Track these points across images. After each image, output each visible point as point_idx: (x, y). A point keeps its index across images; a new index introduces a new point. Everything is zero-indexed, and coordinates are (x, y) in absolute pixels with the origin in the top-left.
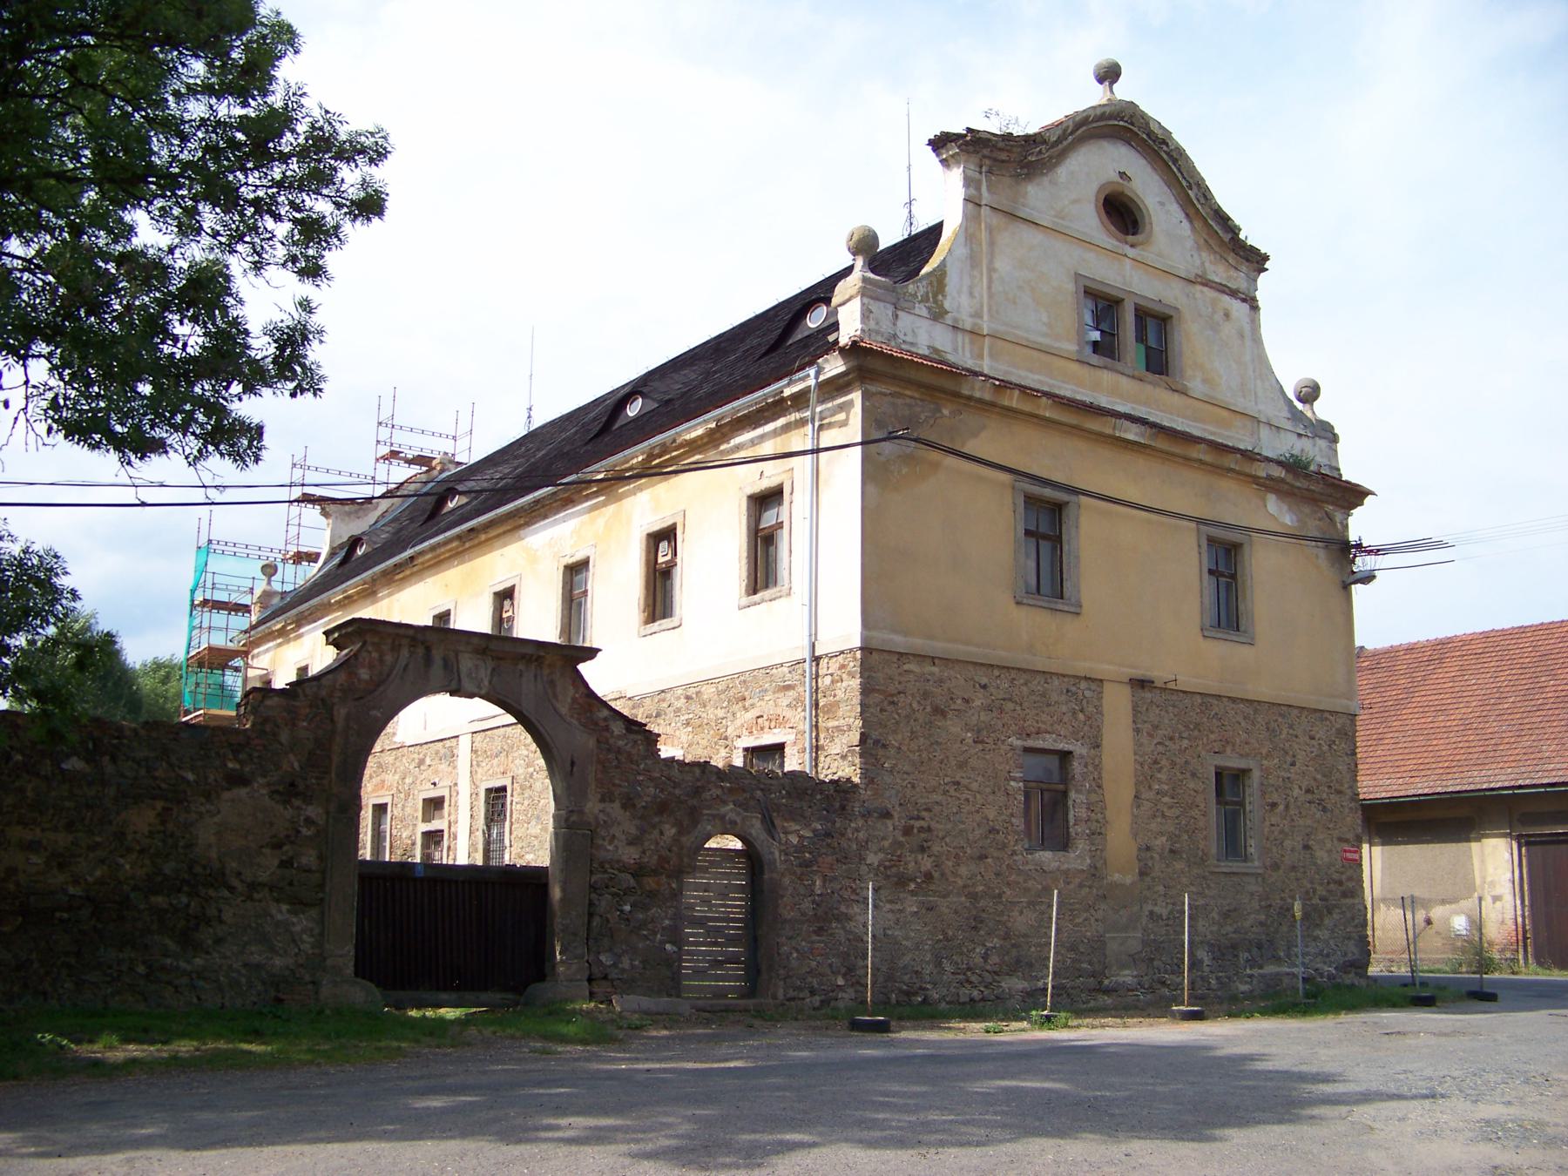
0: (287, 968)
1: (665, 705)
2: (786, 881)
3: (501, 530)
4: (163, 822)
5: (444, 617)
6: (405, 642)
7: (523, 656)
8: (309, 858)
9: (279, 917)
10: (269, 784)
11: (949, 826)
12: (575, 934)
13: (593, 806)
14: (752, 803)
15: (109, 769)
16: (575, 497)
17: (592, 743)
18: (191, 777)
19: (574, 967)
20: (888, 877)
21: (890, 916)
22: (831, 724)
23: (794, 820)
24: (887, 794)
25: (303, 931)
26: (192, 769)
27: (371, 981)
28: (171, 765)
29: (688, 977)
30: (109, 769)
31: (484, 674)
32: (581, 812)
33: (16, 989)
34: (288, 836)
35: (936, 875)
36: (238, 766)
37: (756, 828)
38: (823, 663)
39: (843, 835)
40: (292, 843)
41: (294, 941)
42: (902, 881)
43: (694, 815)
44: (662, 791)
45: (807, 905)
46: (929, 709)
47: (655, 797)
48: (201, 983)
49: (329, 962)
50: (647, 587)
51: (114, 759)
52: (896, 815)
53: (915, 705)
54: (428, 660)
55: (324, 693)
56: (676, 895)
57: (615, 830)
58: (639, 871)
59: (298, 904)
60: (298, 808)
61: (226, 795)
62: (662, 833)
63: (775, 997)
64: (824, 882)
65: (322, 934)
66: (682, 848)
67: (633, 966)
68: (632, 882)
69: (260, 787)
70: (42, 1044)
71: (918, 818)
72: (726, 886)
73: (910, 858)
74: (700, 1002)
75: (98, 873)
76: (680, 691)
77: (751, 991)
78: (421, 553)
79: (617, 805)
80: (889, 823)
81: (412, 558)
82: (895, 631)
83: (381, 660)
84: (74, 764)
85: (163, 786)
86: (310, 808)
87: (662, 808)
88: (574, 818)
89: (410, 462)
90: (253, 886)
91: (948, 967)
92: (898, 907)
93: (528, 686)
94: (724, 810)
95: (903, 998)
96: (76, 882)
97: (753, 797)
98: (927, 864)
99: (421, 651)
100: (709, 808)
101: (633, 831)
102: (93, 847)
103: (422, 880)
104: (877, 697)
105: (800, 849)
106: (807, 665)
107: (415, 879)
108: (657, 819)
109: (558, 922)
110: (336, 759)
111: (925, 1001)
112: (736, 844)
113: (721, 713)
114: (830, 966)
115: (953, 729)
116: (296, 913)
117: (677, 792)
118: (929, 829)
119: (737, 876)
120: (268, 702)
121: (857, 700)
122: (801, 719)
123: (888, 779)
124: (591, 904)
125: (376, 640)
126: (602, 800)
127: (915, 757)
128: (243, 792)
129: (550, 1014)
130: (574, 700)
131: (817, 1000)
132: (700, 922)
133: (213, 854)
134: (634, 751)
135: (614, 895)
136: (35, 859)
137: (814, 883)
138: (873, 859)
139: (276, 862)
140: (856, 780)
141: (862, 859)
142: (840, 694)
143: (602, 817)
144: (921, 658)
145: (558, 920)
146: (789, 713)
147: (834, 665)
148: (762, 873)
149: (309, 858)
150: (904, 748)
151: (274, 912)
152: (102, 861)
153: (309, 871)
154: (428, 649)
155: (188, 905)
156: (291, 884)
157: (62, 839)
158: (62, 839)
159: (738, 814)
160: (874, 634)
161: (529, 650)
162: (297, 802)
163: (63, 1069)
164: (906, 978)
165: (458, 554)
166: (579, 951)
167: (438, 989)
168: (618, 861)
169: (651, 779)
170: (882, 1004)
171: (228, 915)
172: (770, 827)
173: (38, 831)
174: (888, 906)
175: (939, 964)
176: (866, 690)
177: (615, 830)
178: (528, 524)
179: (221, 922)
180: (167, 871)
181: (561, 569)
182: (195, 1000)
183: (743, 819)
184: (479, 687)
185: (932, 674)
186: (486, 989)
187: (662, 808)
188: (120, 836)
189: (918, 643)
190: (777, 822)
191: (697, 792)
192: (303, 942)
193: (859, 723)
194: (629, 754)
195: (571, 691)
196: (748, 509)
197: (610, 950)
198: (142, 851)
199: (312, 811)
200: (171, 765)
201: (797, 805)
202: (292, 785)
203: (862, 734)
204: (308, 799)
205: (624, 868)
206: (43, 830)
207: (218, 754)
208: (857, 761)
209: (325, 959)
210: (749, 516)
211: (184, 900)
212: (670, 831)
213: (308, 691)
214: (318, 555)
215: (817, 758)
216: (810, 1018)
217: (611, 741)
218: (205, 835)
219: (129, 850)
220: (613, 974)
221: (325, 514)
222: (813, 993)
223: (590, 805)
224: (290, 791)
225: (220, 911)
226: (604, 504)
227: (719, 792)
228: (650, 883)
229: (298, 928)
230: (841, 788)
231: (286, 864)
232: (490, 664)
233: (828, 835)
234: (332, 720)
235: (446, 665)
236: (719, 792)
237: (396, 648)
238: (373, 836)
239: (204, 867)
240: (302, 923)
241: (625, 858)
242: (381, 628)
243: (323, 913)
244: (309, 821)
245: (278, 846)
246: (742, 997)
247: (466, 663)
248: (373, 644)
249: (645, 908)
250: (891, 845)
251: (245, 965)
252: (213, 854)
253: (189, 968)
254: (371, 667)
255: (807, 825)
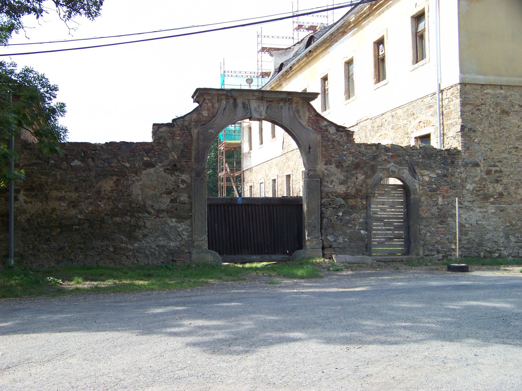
0: (177, 247)
1: (384, 120)
2: (423, 198)
3: (321, 50)
4: (117, 186)
5: (305, 90)
6: (223, 97)
7: (282, 99)
8: (184, 198)
9: (172, 224)
10: (163, 166)
11: (512, 169)
12: (314, 227)
13: (321, 167)
14: (403, 162)
15: (92, 164)
16: (346, 30)
17: (319, 137)
18: (128, 165)
19: (314, 242)
20: (478, 195)
21: (480, 214)
22: (449, 122)
23: (426, 169)
24: (477, 155)
25: (183, 230)
26: (128, 162)
27: (216, 251)
28: (119, 161)
29: (375, 246)
30: (92, 164)
31: (263, 109)
32: (315, 170)
33: (60, 258)
34: (174, 189)
35: (505, 194)
36: (149, 159)
37: (406, 174)
38: (444, 93)
39: (453, 176)
40: (176, 191)
41: (179, 235)
42: (486, 198)
43: (373, 169)
44: (356, 158)
45: (434, 210)
46: (499, 111)
47: (353, 161)
48: (138, 254)
49: (195, 243)
50: (375, 68)
51: (93, 159)
52: (482, 165)
53: (491, 110)
54: (235, 105)
55: (186, 123)
56: (367, 208)
57: (333, 178)
58: (346, 196)
59: (181, 219)
60: (178, 176)
61: (144, 172)
62: (357, 178)
63: (417, 254)
64: (444, 198)
65: (192, 231)
66: (367, 185)
67: (345, 242)
68: (343, 202)
69: (160, 168)
70: (49, 282)
71: (495, 166)
72: (393, 202)
73: (490, 186)
74: (379, 258)
75: (90, 209)
76: (389, 114)
77: (407, 252)
78: (294, 65)
79: (333, 166)
80: (478, 169)
81: (291, 68)
82: (479, 74)
83: (213, 106)
84: (76, 163)
85: (116, 170)
86: (183, 175)
87: (357, 166)
88: (311, 173)
89: (308, 29)
90: (159, 211)
91: (513, 239)
92: (484, 210)
93: (286, 113)
94: (388, 166)
95: (487, 254)
96: (81, 213)
97: (404, 160)
98: (500, 188)
99: (231, 101)
100: (381, 165)
101: (342, 178)
102: (88, 198)
103: (241, 205)
104: (469, 108)
105: (430, 183)
106: (437, 95)
107: (238, 205)
108: (354, 172)
109: (306, 221)
110: (193, 153)
111: (500, 256)
112: (399, 183)
113: (405, 122)
114: (448, 239)
115: (513, 121)
116: (180, 222)
117: (364, 158)
118: (501, 171)
119: (399, 197)
120: (161, 130)
121: (459, 109)
122: (436, 120)
123: (477, 147)
124: (322, 213)
125: (210, 98)
126: (326, 164)
127: (492, 136)
128: (152, 170)
129: (301, 264)
130: (309, 118)
131: (440, 256)
132: (381, 220)
133: (140, 198)
134: (341, 140)
135: (334, 208)
136: (63, 204)
137: (438, 199)
138: (469, 187)
139: (169, 200)
140: (460, 148)
141: (464, 187)
142: (452, 107)
143: (326, 172)
144: (494, 86)
145: (306, 221)
146: (431, 119)
147: (449, 92)
148: (410, 196)
149: (184, 198)
150: (486, 132)
151: (169, 222)
152: (91, 204)
153: (185, 203)
154: (235, 100)
155: (130, 221)
156: (176, 209)
157: (74, 195)
158: (74, 195)
159: (396, 167)
160: (467, 76)
161: (284, 96)
162: (177, 173)
163: (61, 292)
164: (489, 245)
165: (307, 63)
166: (317, 235)
167: (252, 254)
168: (335, 192)
169: (350, 153)
170: (464, 258)
171: (148, 224)
172: (413, 173)
173: (63, 192)
174: (479, 209)
175: (507, 238)
176: (463, 104)
177: (333, 178)
178: (330, 46)
179: (145, 227)
180: (120, 207)
181: (344, 64)
182: (136, 262)
183: (399, 170)
184: (261, 115)
185: (501, 94)
186: (275, 253)
187: (357, 166)
188: (99, 192)
189: (491, 79)
190: (417, 171)
191: (374, 158)
192: (183, 235)
193: (460, 121)
194: (338, 142)
195: (307, 114)
196: (412, 23)
197: (333, 234)
198: (108, 198)
199: (184, 177)
200: (119, 161)
201: (428, 162)
202: (175, 166)
203: (462, 126)
204: (182, 172)
205: (338, 196)
206: (65, 192)
207: (139, 154)
208: (460, 139)
209: (194, 242)
210: (412, 26)
211: (129, 219)
212: (361, 177)
213: (179, 123)
214: (270, 73)
215: (443, 139)
216: (435, 264)
217: (329, 136)
218: (136, 190)
219: (103, 198)
220: (334, 245)
221: (271, 55)
222: (438, 252)
223: (319, 166)
224: (173, 168)
225: (145, 223)
226: (357, 32)
227: (386, 157)
228: (352, 202)
229: (180, 229)
230: (452, 153)
231: (172, 201)
232: (265, 105)
233: (445, 176)
234: (191, 136)
235: (244, 106)
236: (386, 157)
237: (219, 101)
238: (287, 189)
239: (137, 204)
240: (182, 227)
241: (339, 191)
242: (210, 92)
243: (192, 222)
244: (183, 181)
245: (169, 193)
246: (403, 254)
247: (254, 104)
248: (208, 99)
249: (350, 214)
250: (479, 180)
251: (157, 246)
252: (140, 198)
253: (132, 248)
254: (208, 110)
255: (434, 171)
